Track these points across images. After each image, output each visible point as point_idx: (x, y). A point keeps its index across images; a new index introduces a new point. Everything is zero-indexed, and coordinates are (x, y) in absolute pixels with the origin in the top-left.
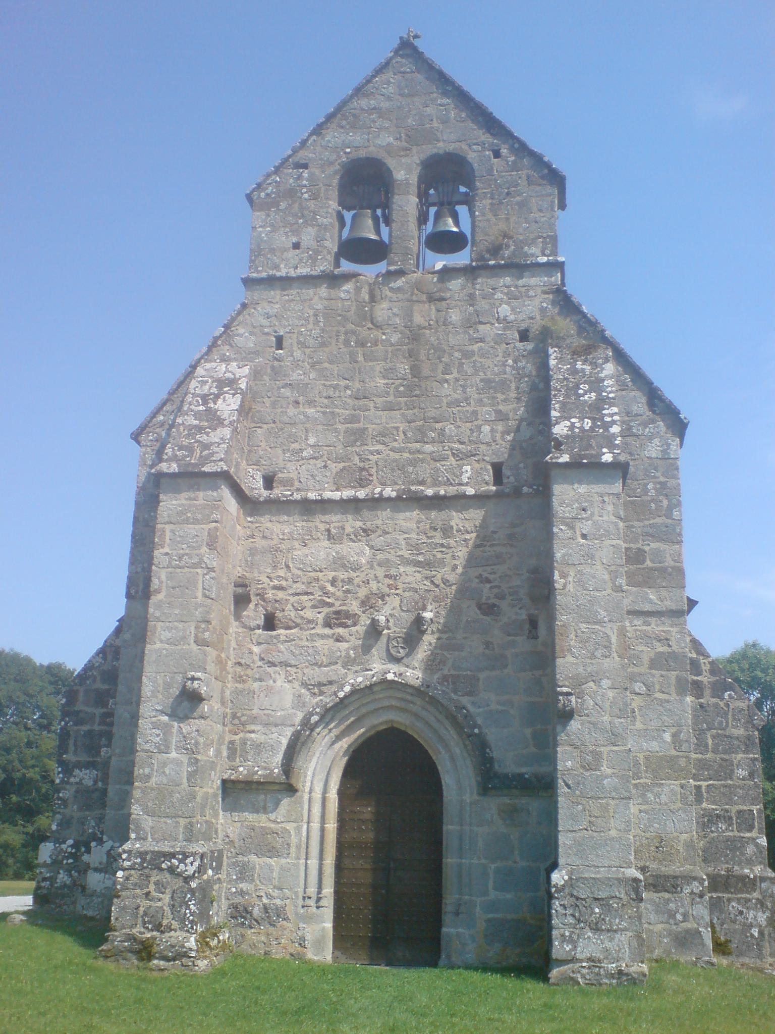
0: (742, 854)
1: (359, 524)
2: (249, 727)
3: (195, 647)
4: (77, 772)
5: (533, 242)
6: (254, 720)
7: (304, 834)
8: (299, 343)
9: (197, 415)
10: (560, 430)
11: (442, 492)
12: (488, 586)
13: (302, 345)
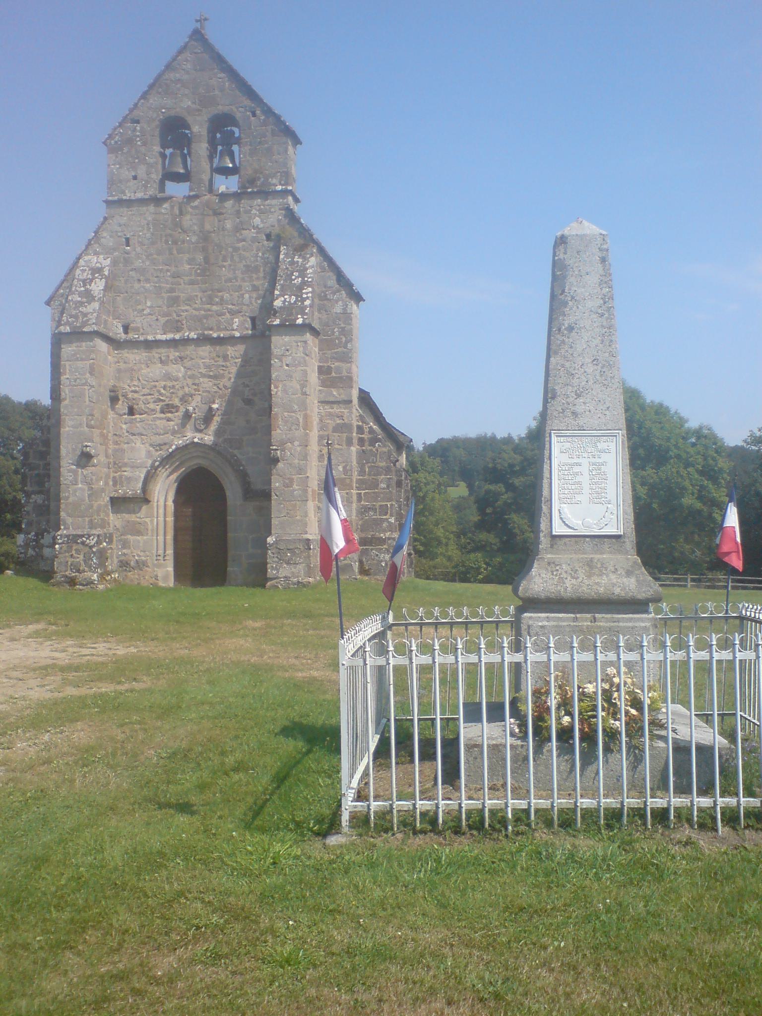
0: (381, 527)
1: (177, 354)
2: (123, 469)
3: (86, 428)
4: (33, 496)
5: (273, 176)
6: (126, 465)
7: (155, 524)
8: (139, 242)
9: (80, 294)
10: (278, 303)
11: (222, 335)
12: (248, 388)
13: (141, 244)
